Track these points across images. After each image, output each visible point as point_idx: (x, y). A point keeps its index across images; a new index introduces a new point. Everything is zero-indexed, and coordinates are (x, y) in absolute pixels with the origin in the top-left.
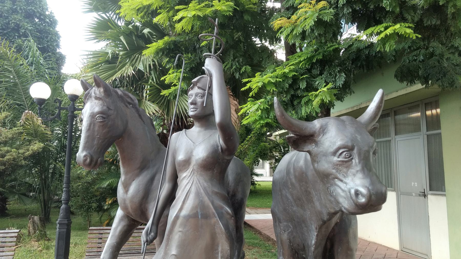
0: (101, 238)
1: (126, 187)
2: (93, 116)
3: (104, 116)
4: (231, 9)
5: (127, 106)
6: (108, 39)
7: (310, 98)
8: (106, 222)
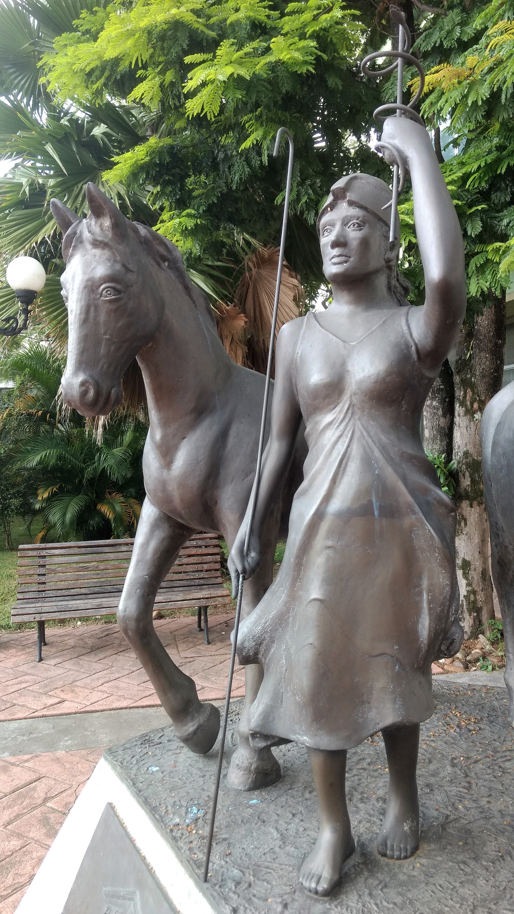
0: (44, 566)
1: (167, 453)
2: (91, 287)
3: (118, 287)
4: (310, 58)
5: (159, 264)
6: (19, 153)
7: (490, 257)
8: (41, 535)
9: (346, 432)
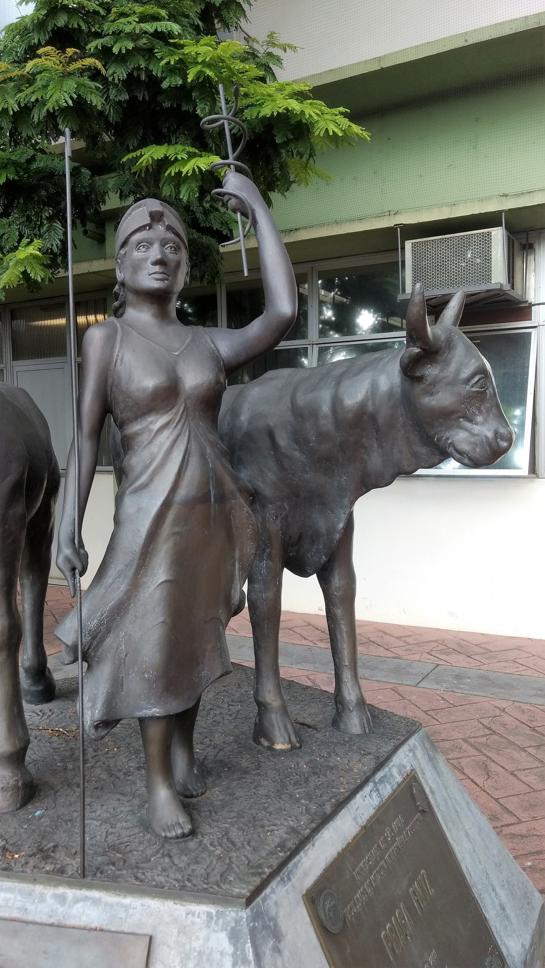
9: (183, 431)
